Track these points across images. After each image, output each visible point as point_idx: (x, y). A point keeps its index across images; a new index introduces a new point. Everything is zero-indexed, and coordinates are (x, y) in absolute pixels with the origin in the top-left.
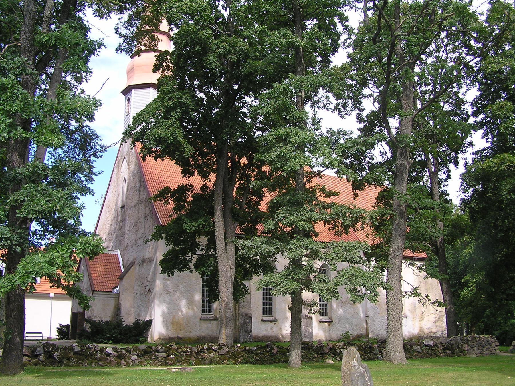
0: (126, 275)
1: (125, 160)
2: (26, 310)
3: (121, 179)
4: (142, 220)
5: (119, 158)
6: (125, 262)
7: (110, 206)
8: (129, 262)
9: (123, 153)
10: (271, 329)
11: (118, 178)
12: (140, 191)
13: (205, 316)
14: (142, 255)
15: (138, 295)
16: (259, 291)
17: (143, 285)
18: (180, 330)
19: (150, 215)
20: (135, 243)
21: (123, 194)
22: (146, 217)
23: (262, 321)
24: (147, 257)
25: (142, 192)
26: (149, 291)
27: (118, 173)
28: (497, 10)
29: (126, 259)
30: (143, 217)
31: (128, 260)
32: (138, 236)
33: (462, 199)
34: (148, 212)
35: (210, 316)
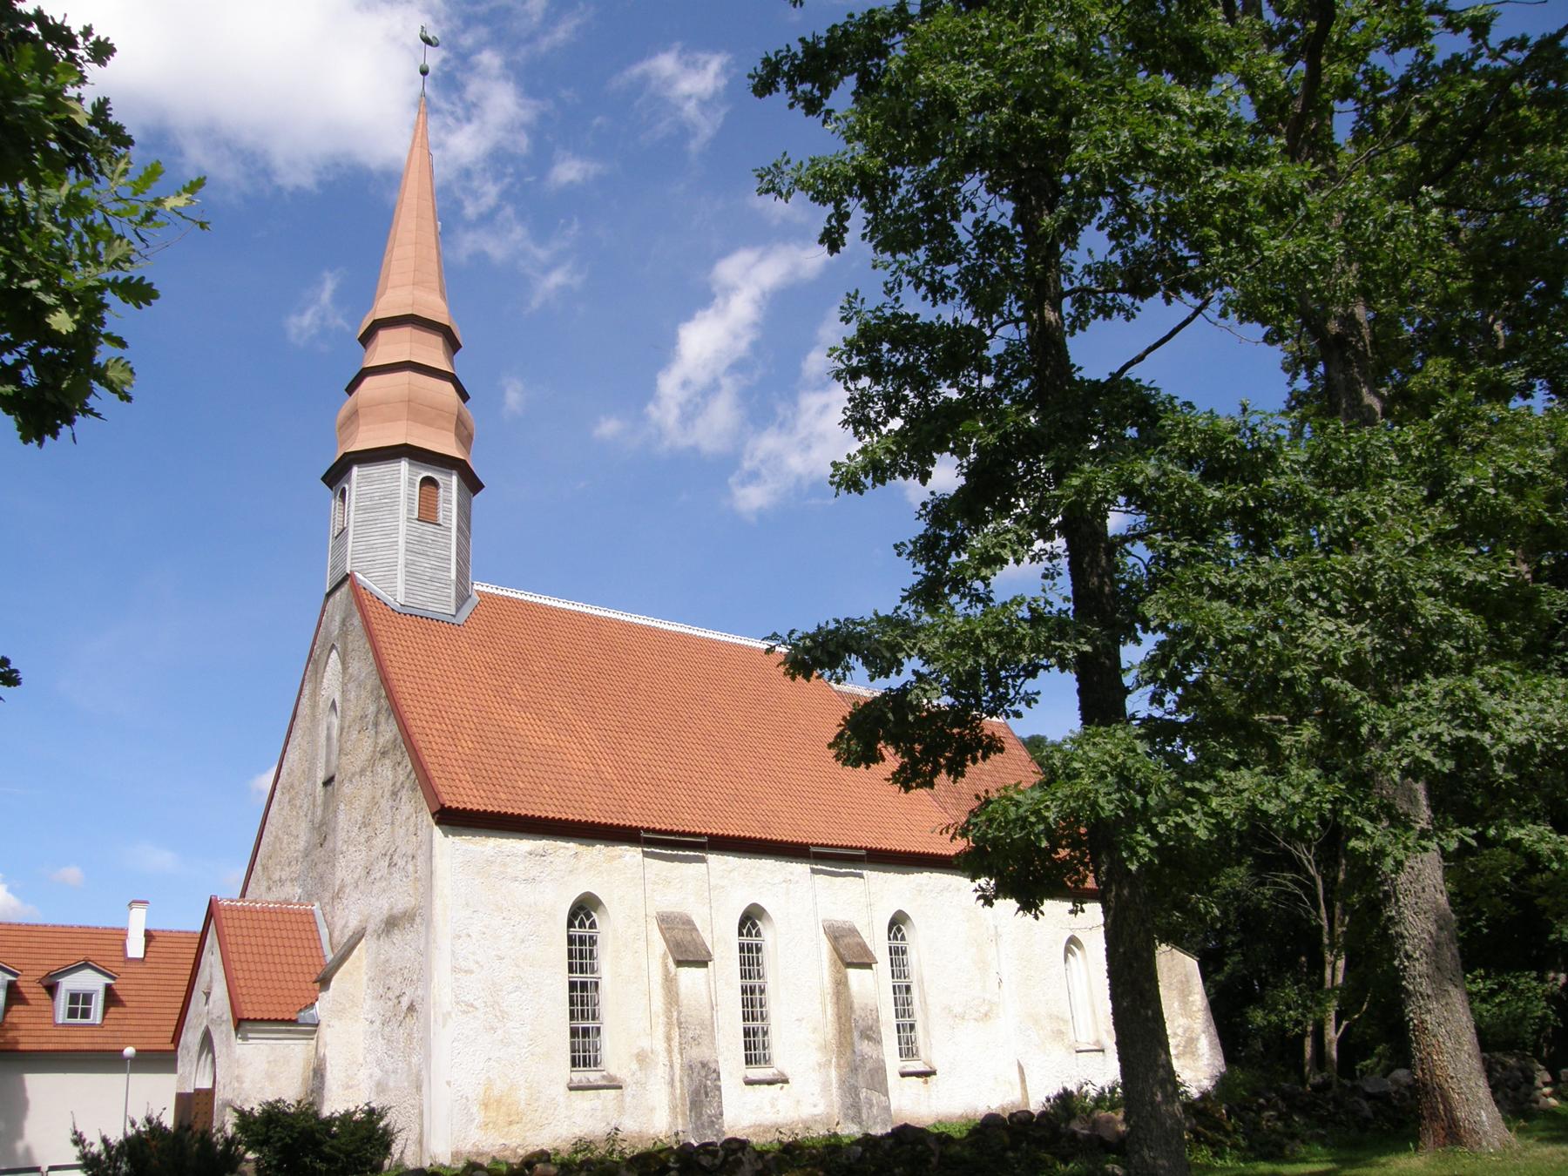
0: (342, 969)
1: (334, 655)
2: (1105, 966)
3: (323, 704)
4: (385, 804)
5: (317, 651)
6: (336, 934)
7: (292, 786)
8: (349, 933)
9: (328, 633)
10: (773, 1106)
11: (314, 706)
12: (376, 724)
13: (582, 1076)
14: (386, 906)
15: (378, 1023)
16: (1076, 961)
17: (390, 994)
18: (511, 1123)
19: (407, 785)
20: (364, 873)
21: (329, 738)
22: (394, 794)
23: (749, 1083)
24: (400, 907)
25: (382, 728)
26: (411, 1008)
27: (314, 694)
28: (1565, 50)
29: (339, 924)
30: (387, 795)
31: (345, 926)
32: (374, 853)
33: (1436, 677)
34: (402, 778)
35: (592, 1076)
